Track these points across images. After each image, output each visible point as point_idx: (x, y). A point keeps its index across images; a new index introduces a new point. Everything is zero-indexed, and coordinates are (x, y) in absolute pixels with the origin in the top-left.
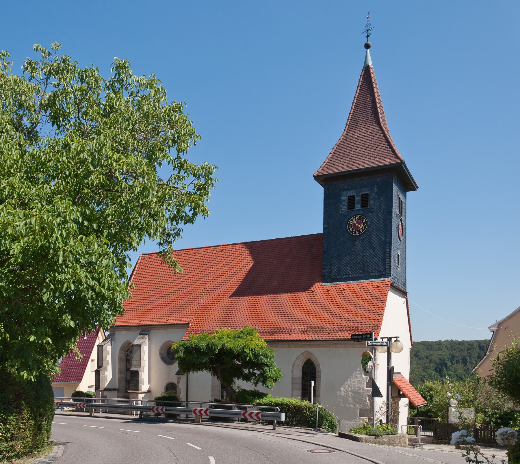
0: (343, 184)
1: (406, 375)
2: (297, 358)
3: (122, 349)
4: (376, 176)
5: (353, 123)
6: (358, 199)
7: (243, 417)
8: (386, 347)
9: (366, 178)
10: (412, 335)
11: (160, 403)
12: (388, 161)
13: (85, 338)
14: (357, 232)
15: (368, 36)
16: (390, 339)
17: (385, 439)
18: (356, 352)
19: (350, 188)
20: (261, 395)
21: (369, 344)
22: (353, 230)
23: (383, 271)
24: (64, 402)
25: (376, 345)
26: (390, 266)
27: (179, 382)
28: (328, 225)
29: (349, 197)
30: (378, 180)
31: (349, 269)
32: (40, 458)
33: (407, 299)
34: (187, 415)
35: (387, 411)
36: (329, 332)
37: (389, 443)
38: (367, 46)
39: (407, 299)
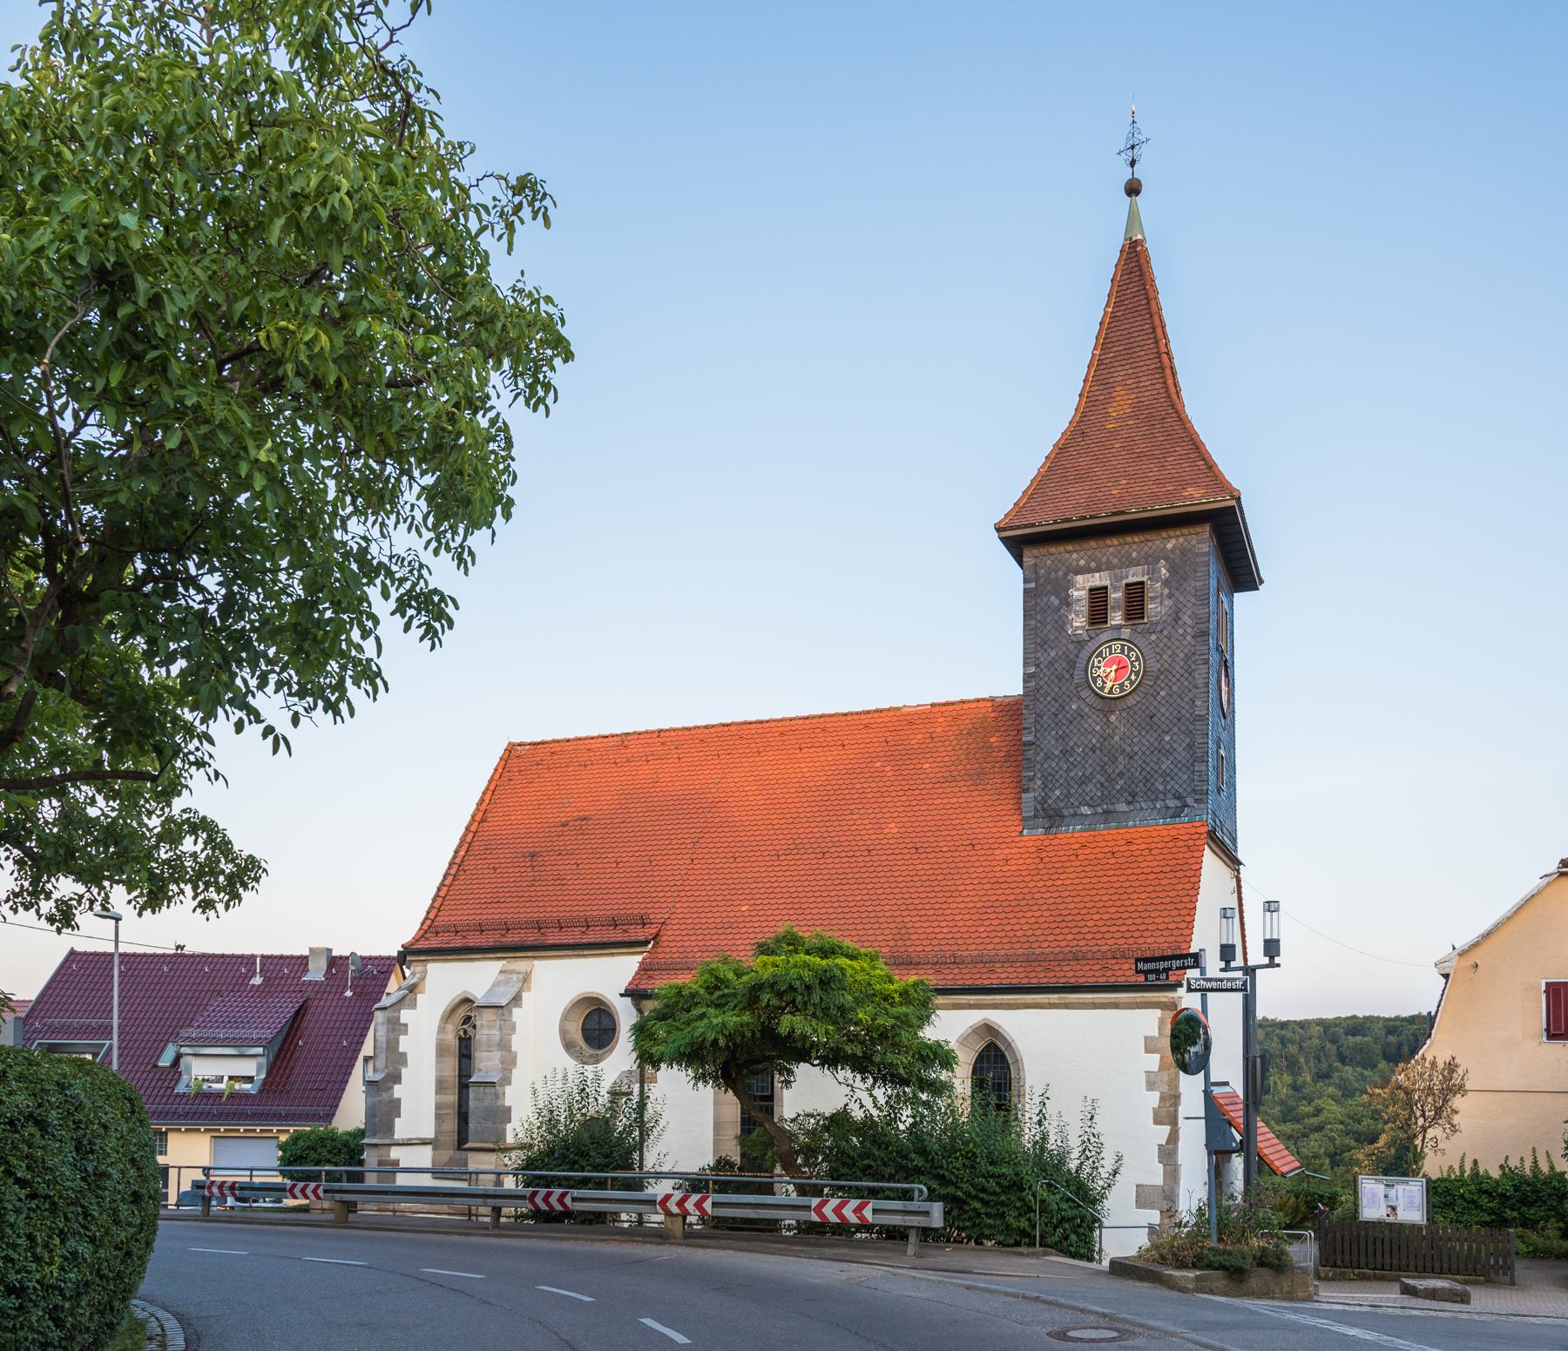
0: (1075, 556)
4: (1164, 534)
6: (1116, 596)
8: (1240, 995)
13: (349, 993)
15: (1133, 163)
19: (1093, 565)
24: (255, 1180)
28: (1037, 666)
30: (1169, 546)
32: (768, 1189)
34: (640, 1215)
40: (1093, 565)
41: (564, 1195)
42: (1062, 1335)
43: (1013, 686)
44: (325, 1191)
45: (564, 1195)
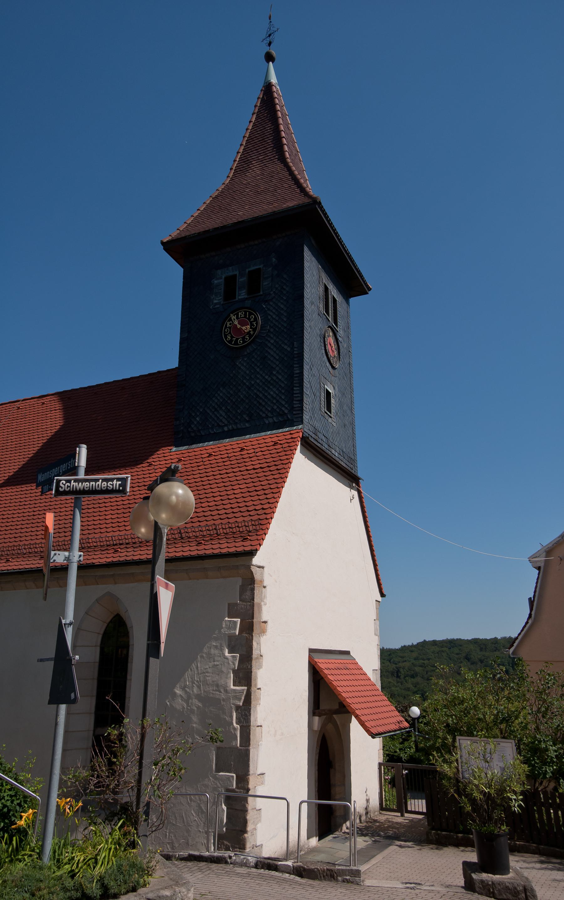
5: (243, 165)
6: (242, 280)
9: (256, 242)
10: (379, 572)
12: (293, 201)
14: (240, 341)
15: (270, 44)
21: (63, 485)
22: (232, 337)
26: (301, 401)
29: (226, 279)
31: (224, 414)
38: (269, 58)
39: (360, 493)
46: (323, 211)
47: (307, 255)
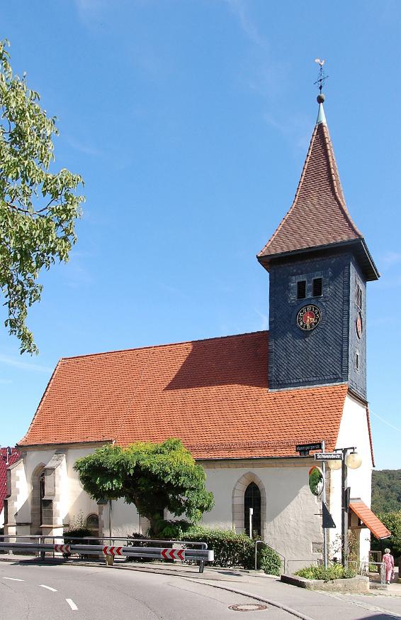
0: (292, 268)
1: (367, 500)
2: (238, 481)
3: (35, 474)
5: (304, 193)
6: (309, 285)
7: (162, 556)
8: (341, 461)
9: (318, 259)
11: (69, 540)
15: (321, 88)
16: (345, 451)
17: (340, 583)
18: (304, 472)
19: (299, 271)
20: (185, 526)
21: (319, 457)
23: (340, 374)
25: (329, 459)
27: (100, 513)
30: (333, 262)
33: (367, 410)
35: (343, 546)
36: (275, 448)
37: (346, 589)
38: (320, 100)
39: (367, 410)
40: (299, 271)
41: (68, 546)
42: (235, 608)
43: (265, 327)
44: (186, 554)
45: (68, 546)
46: (364, 244)
47: (351, 265)
